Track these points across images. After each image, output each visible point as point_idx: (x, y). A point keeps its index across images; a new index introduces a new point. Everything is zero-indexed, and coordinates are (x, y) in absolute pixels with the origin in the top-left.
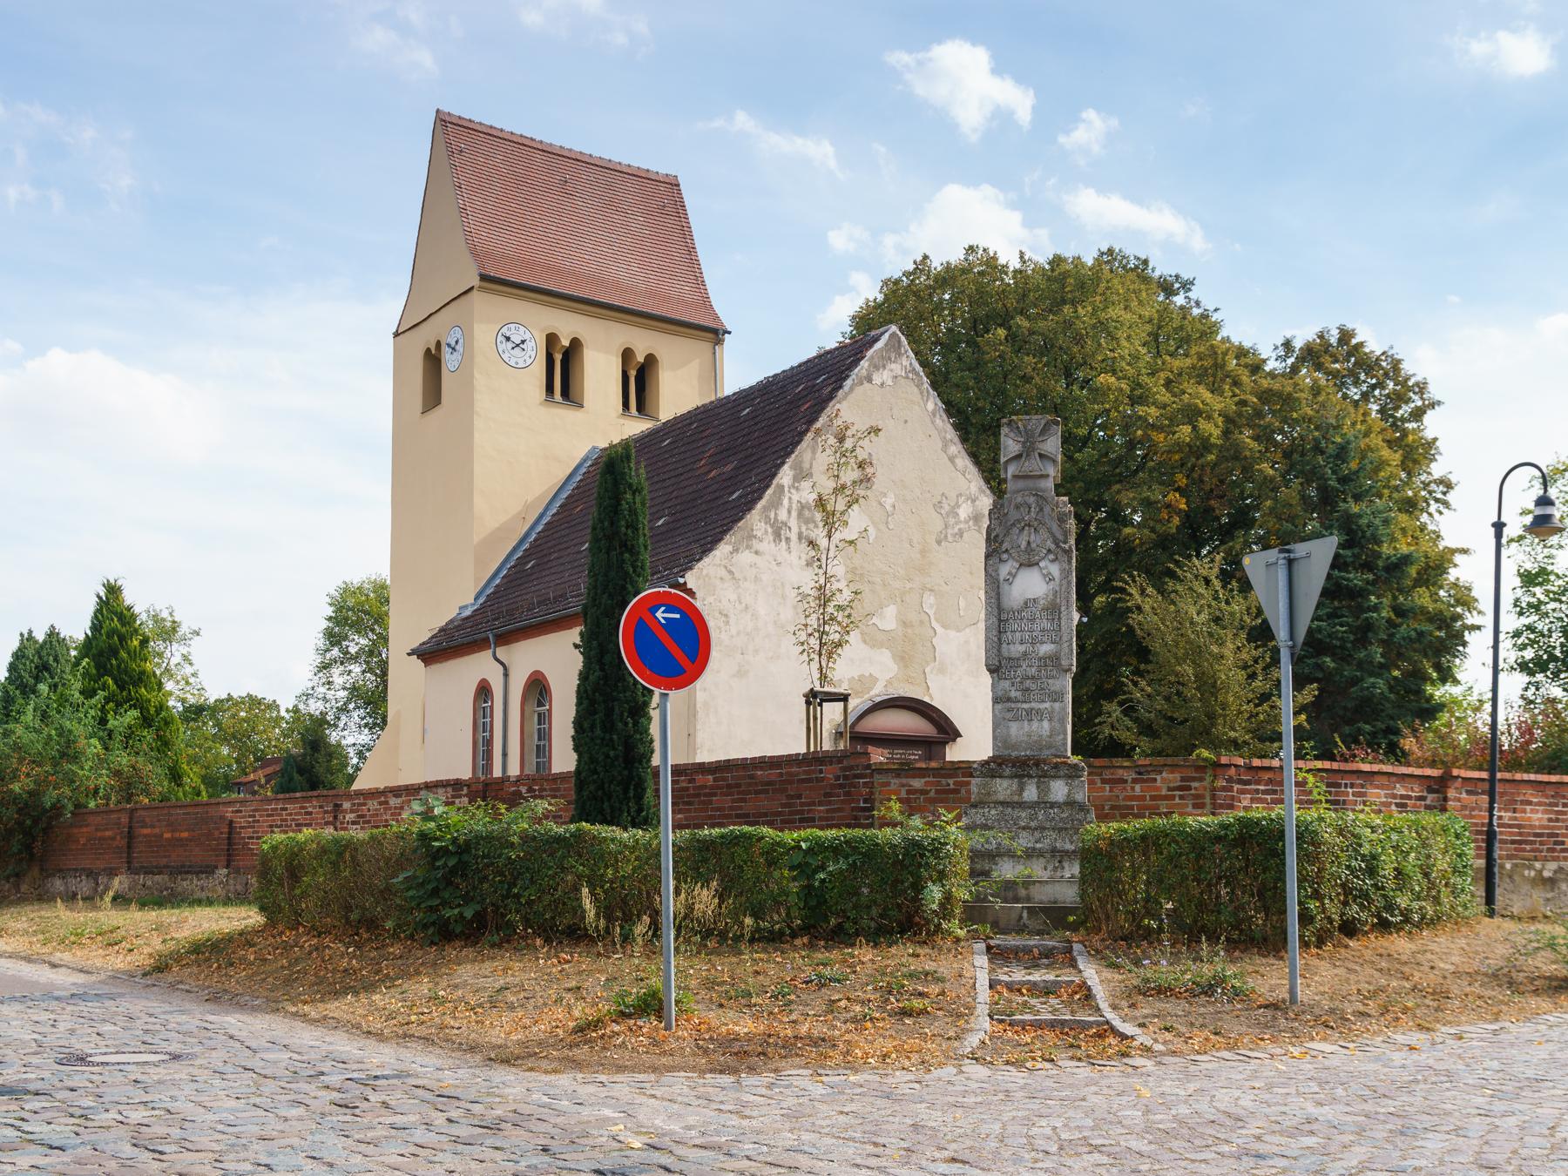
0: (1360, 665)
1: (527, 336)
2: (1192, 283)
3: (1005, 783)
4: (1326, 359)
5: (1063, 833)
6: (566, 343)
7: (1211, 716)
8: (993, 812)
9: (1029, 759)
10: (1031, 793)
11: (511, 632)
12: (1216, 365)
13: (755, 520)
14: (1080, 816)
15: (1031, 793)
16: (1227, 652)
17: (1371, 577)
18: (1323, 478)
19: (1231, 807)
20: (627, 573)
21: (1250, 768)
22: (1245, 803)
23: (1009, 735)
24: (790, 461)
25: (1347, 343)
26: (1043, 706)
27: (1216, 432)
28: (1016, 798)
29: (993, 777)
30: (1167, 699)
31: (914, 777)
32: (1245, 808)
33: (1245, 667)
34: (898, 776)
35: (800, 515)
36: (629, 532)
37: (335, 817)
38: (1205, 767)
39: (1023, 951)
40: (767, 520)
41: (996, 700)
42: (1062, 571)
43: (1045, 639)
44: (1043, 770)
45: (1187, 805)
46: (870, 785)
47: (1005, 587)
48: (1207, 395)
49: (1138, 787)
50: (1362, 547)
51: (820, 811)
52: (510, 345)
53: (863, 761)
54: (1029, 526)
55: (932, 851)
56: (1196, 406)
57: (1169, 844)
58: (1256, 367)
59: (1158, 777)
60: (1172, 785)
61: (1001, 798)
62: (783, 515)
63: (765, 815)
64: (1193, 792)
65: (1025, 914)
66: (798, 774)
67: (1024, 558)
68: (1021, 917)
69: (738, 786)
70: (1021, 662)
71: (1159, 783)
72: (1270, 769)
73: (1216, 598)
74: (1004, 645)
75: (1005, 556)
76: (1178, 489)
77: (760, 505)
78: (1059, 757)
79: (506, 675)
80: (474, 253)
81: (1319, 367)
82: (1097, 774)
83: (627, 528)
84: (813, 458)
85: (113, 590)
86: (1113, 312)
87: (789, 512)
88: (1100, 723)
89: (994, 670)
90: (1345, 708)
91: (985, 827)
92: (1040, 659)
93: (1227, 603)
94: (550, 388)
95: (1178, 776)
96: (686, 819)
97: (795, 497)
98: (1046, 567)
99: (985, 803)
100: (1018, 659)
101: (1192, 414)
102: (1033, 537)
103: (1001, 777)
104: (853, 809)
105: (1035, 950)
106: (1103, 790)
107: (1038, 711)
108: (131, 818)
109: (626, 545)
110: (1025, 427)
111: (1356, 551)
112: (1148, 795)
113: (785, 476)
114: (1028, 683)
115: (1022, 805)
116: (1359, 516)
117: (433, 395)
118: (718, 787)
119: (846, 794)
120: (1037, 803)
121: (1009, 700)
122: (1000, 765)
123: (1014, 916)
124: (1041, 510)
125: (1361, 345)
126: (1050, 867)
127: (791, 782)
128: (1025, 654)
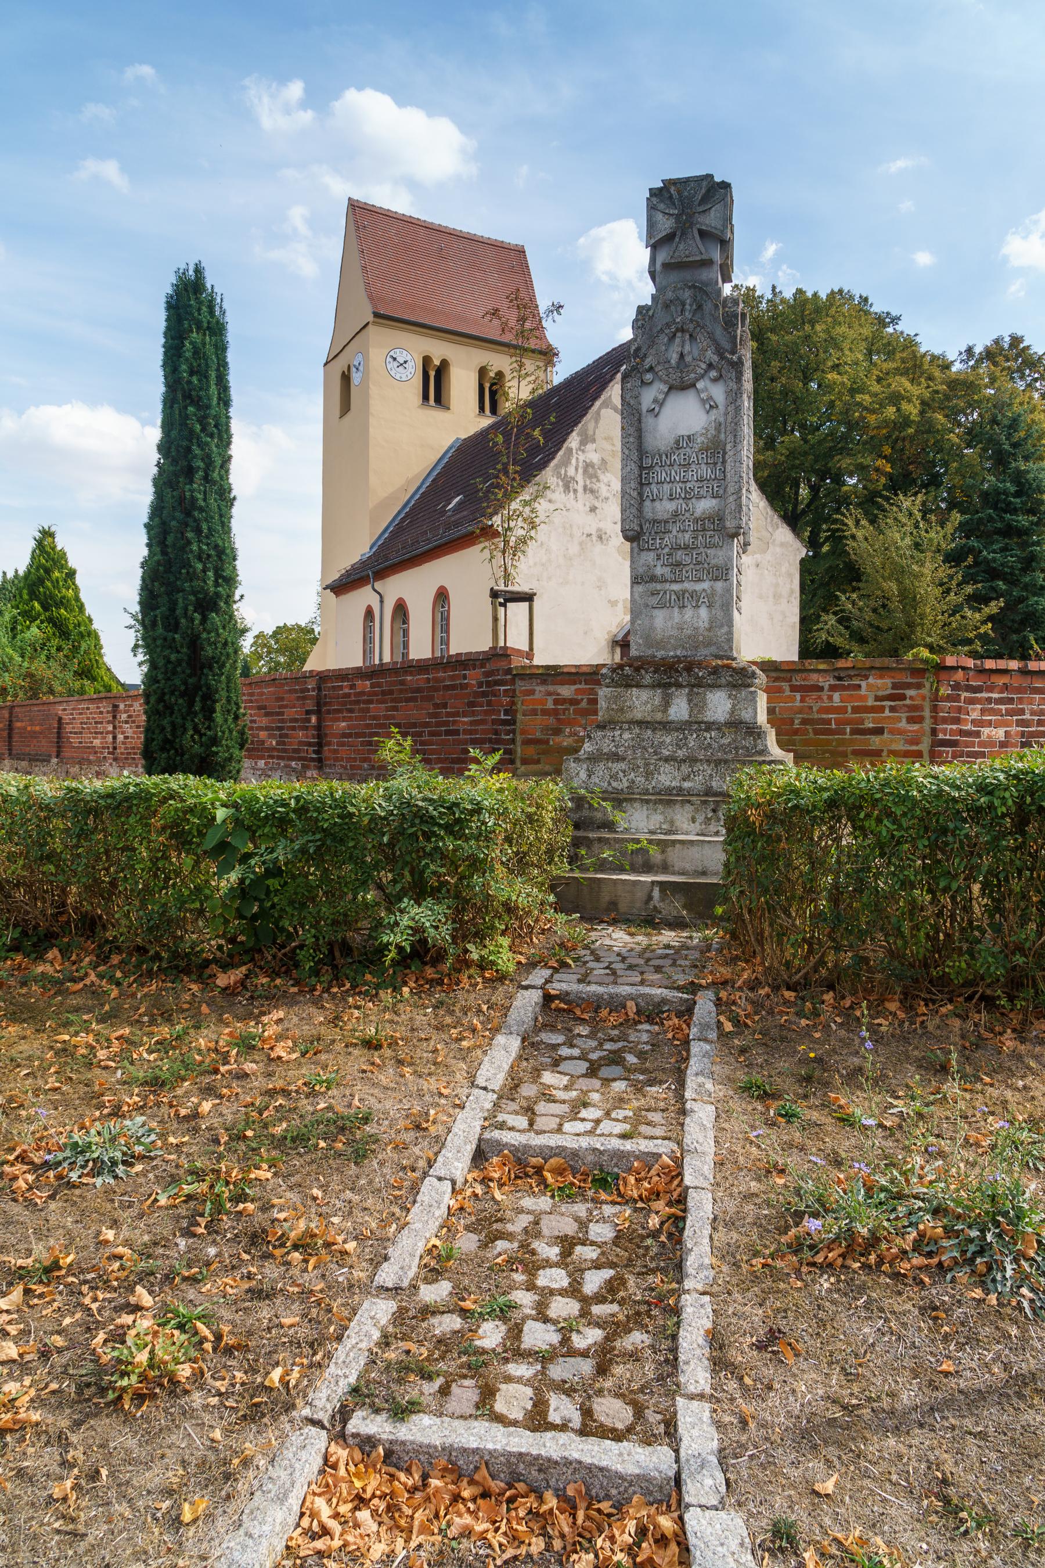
0: (1025, 588)
1: (409, 358)
2: (899, 319)
3: (644, 695)
4: (1000, 359)
5: (722, 768)
6: (437, 362)
7: (911, 625)
8: (626, 736)
9: (679, 662)
10: (680, 709)
11: (387, 568)
12: (915, 365)
13: (549, 475)
14: (748, 742)
15: (680, 709)
16: (926, 571)
17: (1035, 519)
18: (999, 443)
19: (957, 721)
20: (192, 431)
21: (981, 671)
22: (975, 715)
23: (652, 628)
24: (577, 429)
25: (1016, 347)
26: (699, 587)
27: (915, 412)
28: (659, 716)
29: (628, 686)
30: (875, 610)
31: (562, 684)
32: (973, 722)
33: (941, 585)
34: (544, 682)
35: (585, 471)
36: (195, 380)
37: (114, 717)
38: (924, 670)
39: (609, 1004)
40: (559, 476)
41: (636, 580)
42: (728, 393)
43: (703, 492)
44: (697, 677)
45: (899, 719)
46: (512, 693)
47: (649, 421)
48: (907, 384)
49: (836, 696)
50: (1029, 496)
51: (464, 723)
52: (396, 364)
53: (503, 664)
54: (683, 331)
55: (448, 828)
56: (899, 392)
57: (879, 821)
58: (947, 366)
59: (863, 684)
60: (880, 693)
61: (639, 716)
62: (571, 471)
63: (414, 725)
64: (908, 702)
65: (656, 893)
66: (444, 680)
67: (675, 377)
68: (650, 898)
69: (391, 692)
70: (670, 526)
71: (863, 692)
72: (1005, 672)
73: (917, 527)
74: (647, 503)
75: (649, 377)
76: (885, 457)
77: (553, 464)
78: (721, 658)
79: (382, 602)
80: (371, 298)
81: (995, 364)
82: (784, 680)
83: (192, 373)
84: (596, 427)
85: (47, 534)
86: (842, 329)
87: (577, 469)
88: (818, 630)
89: (633, 536)
90: (1013, 621)
91: (616, 757)
92: (696, 520)
93: (927, 532)
94: (426, 397)
95: (888, 681)
96: (349, 727)
97: (582, 458)
98: (706, 389)
99: (615, 723)
100: (666, 522)
101: (895, 399)
102: (687, 348)
103: (638, 686)
104: (494, 722)
105: (631, 1005)
106: (793, 699)
107: (693, 594)
108: (11, 713)
109: (190, 397)
110: (679, 192)
111: (1024, 498)
112: (849, 706)
113: (573, 441)
114: (680, 555)
115: (666, 726)
116: (1028, 472)
117: (346, 406)
118: (375, 694)
119: (489, 703)
120: (688, 723)
121: (653, 579)
122: (637, 670)
123: (640, 895)
124: (700, 307)
125: (1028, 347)
126: (700, 818)
127: (436, 689)
128: (676, 514)
